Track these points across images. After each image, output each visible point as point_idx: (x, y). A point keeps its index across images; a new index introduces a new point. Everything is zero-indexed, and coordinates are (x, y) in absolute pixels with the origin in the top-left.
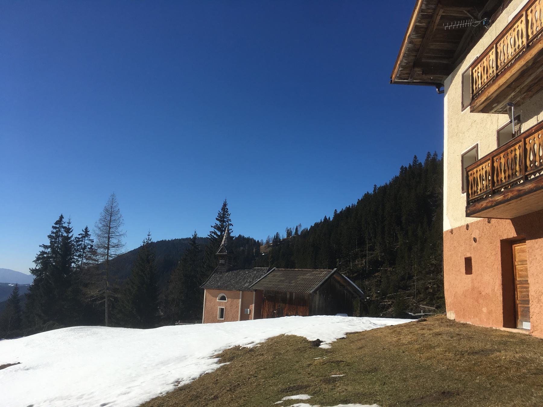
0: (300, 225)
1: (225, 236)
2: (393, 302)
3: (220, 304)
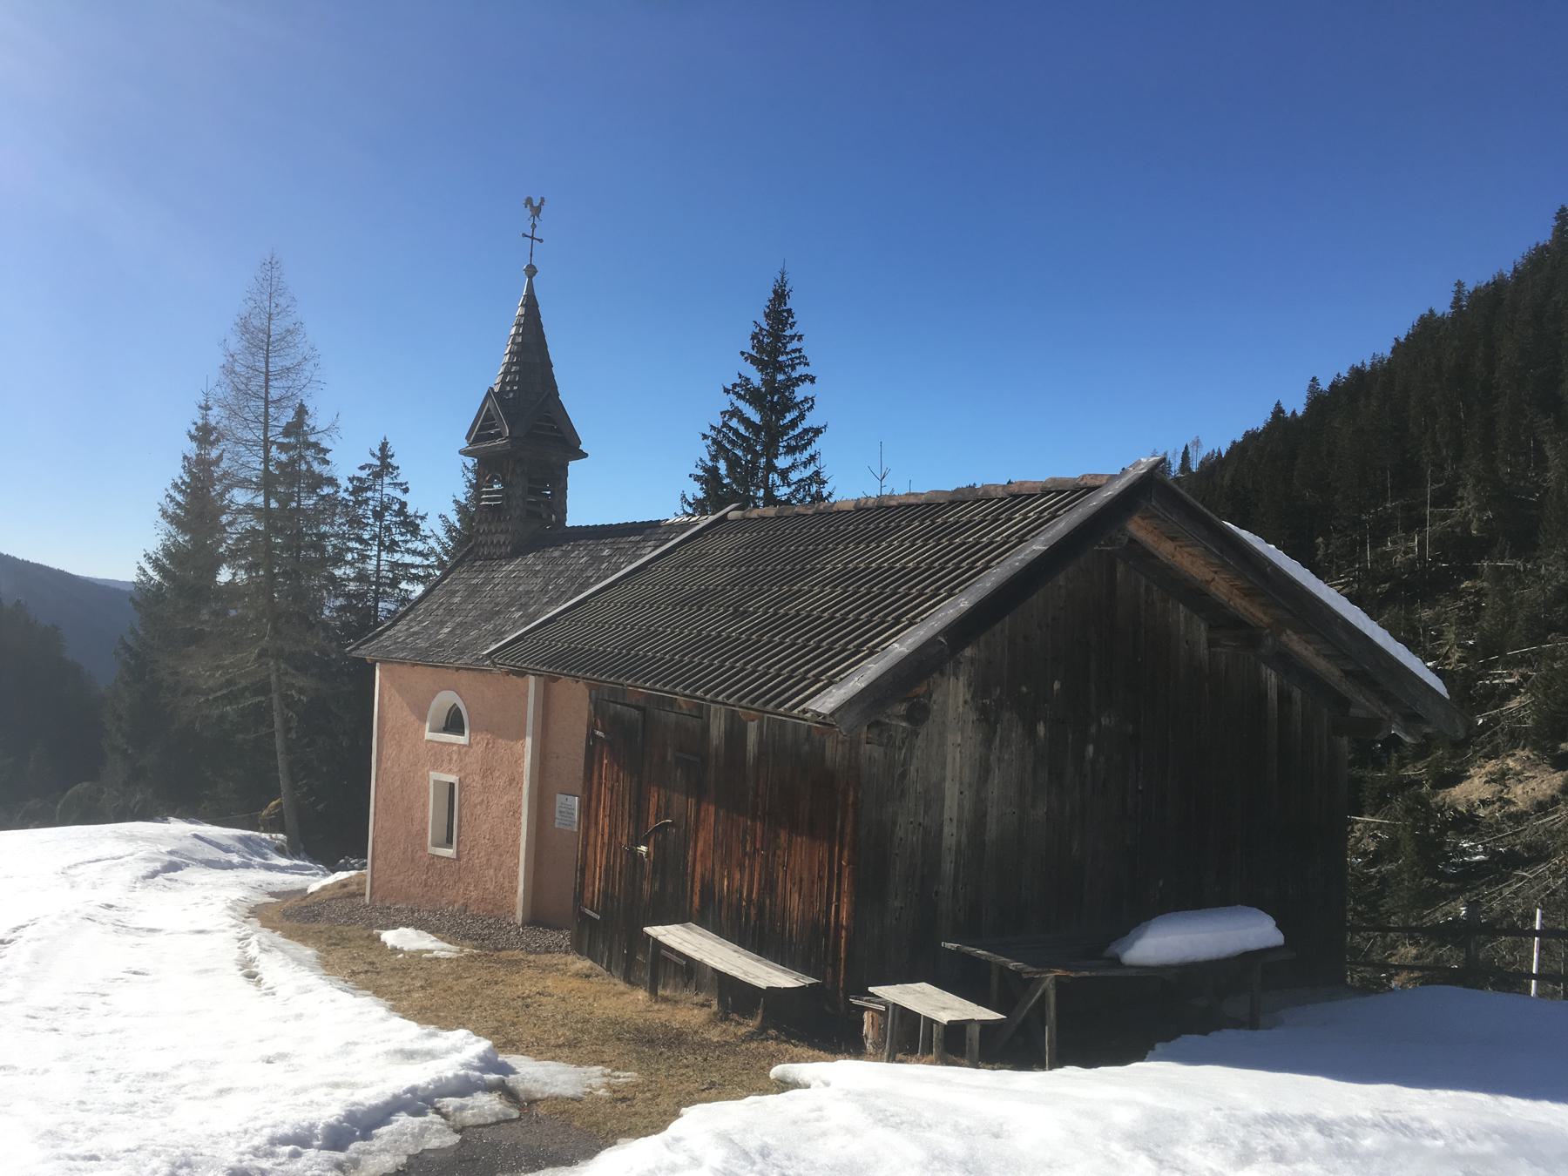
0: (1197, 443)
2: (1525, 678)
3: (439, 756)
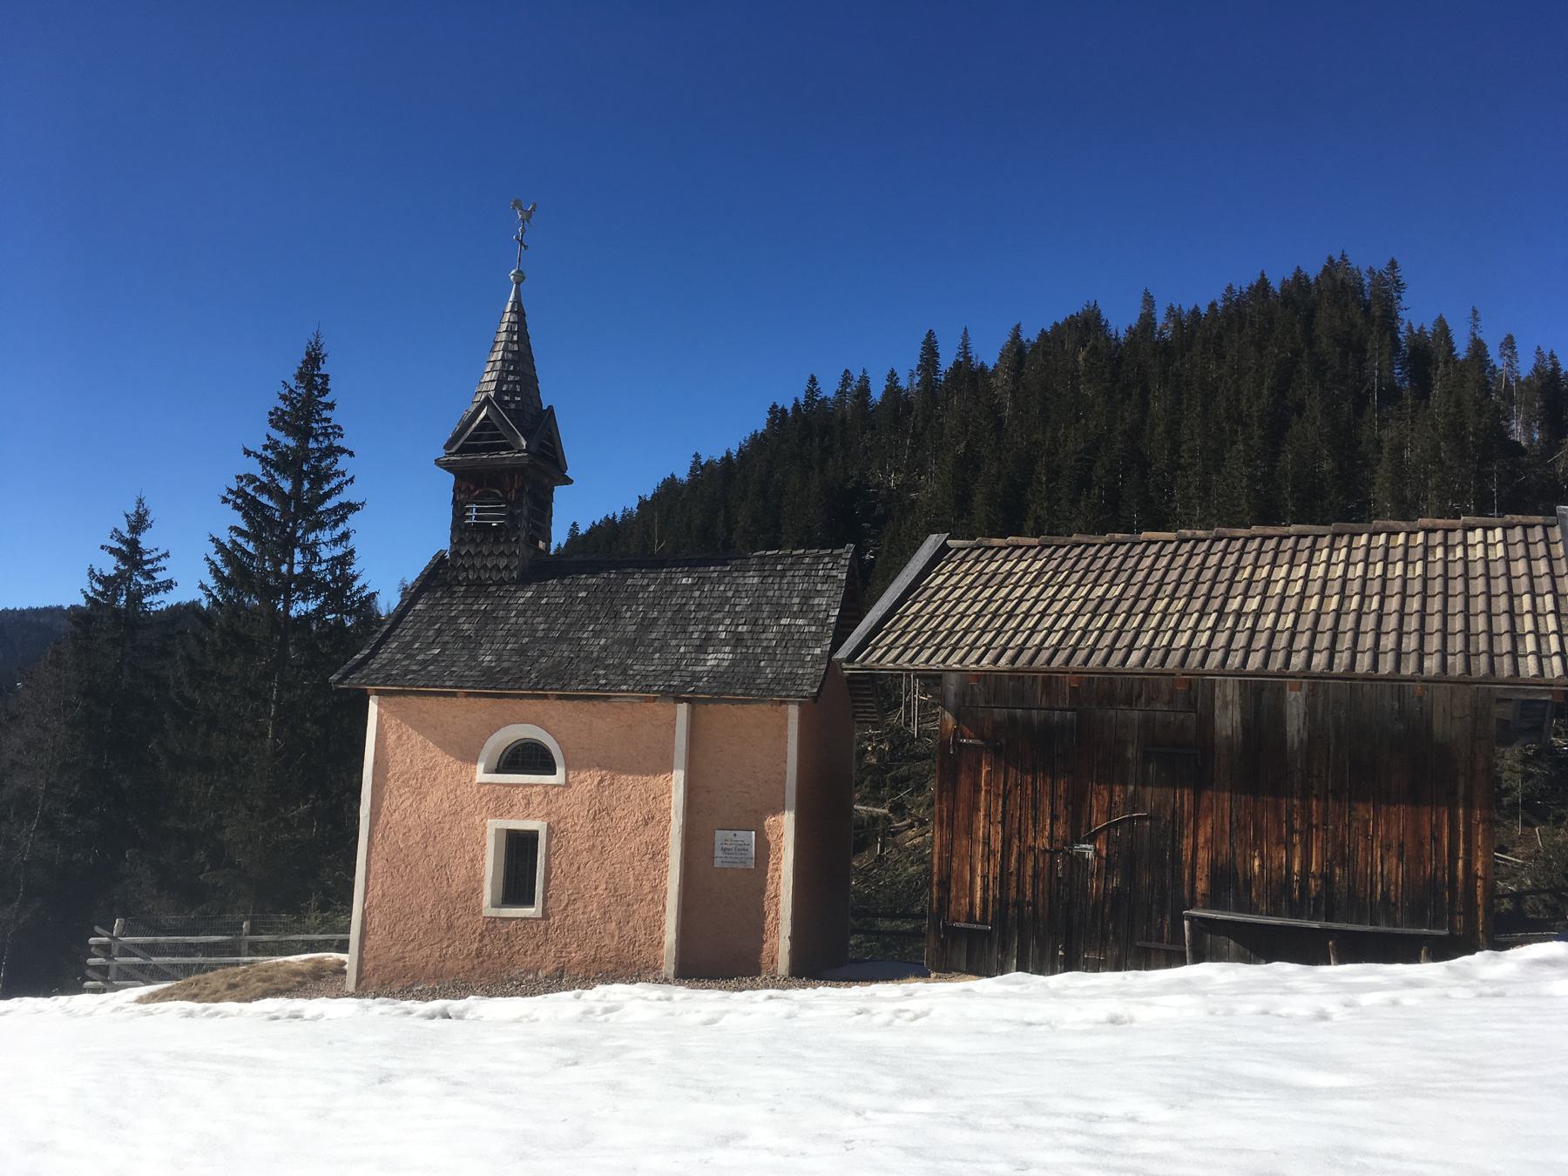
1: (500, 347)
3: (500, 802)
